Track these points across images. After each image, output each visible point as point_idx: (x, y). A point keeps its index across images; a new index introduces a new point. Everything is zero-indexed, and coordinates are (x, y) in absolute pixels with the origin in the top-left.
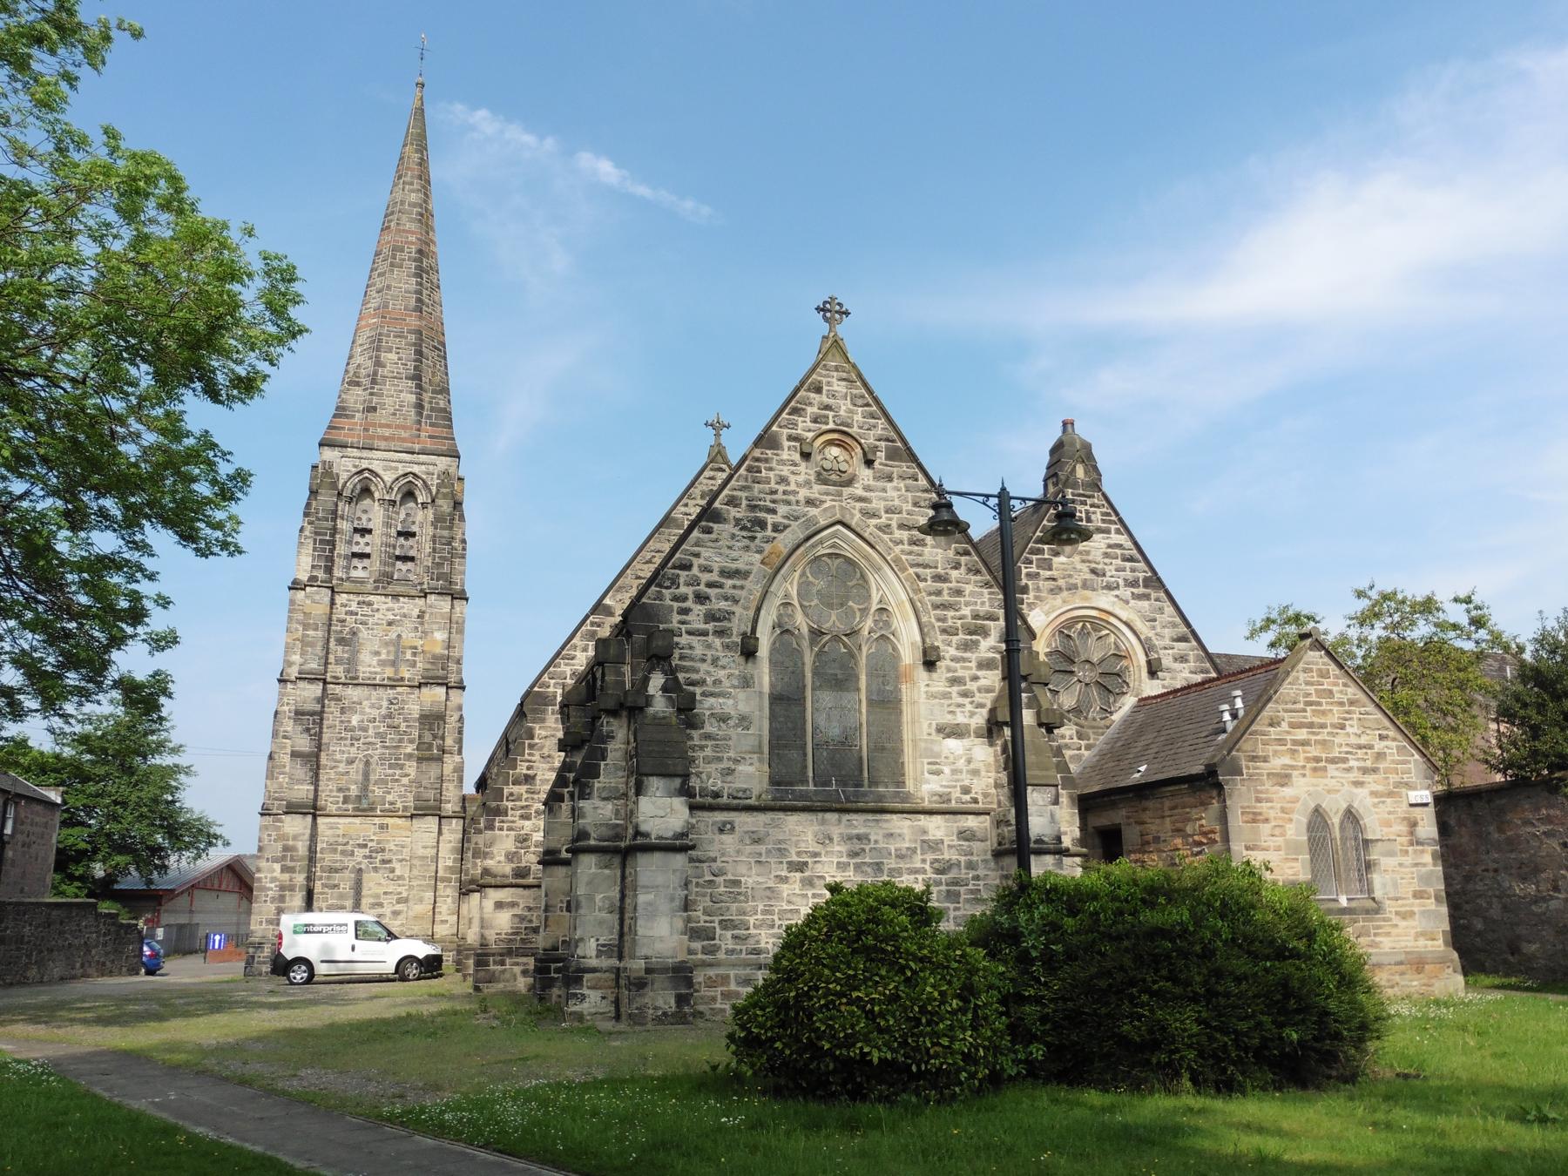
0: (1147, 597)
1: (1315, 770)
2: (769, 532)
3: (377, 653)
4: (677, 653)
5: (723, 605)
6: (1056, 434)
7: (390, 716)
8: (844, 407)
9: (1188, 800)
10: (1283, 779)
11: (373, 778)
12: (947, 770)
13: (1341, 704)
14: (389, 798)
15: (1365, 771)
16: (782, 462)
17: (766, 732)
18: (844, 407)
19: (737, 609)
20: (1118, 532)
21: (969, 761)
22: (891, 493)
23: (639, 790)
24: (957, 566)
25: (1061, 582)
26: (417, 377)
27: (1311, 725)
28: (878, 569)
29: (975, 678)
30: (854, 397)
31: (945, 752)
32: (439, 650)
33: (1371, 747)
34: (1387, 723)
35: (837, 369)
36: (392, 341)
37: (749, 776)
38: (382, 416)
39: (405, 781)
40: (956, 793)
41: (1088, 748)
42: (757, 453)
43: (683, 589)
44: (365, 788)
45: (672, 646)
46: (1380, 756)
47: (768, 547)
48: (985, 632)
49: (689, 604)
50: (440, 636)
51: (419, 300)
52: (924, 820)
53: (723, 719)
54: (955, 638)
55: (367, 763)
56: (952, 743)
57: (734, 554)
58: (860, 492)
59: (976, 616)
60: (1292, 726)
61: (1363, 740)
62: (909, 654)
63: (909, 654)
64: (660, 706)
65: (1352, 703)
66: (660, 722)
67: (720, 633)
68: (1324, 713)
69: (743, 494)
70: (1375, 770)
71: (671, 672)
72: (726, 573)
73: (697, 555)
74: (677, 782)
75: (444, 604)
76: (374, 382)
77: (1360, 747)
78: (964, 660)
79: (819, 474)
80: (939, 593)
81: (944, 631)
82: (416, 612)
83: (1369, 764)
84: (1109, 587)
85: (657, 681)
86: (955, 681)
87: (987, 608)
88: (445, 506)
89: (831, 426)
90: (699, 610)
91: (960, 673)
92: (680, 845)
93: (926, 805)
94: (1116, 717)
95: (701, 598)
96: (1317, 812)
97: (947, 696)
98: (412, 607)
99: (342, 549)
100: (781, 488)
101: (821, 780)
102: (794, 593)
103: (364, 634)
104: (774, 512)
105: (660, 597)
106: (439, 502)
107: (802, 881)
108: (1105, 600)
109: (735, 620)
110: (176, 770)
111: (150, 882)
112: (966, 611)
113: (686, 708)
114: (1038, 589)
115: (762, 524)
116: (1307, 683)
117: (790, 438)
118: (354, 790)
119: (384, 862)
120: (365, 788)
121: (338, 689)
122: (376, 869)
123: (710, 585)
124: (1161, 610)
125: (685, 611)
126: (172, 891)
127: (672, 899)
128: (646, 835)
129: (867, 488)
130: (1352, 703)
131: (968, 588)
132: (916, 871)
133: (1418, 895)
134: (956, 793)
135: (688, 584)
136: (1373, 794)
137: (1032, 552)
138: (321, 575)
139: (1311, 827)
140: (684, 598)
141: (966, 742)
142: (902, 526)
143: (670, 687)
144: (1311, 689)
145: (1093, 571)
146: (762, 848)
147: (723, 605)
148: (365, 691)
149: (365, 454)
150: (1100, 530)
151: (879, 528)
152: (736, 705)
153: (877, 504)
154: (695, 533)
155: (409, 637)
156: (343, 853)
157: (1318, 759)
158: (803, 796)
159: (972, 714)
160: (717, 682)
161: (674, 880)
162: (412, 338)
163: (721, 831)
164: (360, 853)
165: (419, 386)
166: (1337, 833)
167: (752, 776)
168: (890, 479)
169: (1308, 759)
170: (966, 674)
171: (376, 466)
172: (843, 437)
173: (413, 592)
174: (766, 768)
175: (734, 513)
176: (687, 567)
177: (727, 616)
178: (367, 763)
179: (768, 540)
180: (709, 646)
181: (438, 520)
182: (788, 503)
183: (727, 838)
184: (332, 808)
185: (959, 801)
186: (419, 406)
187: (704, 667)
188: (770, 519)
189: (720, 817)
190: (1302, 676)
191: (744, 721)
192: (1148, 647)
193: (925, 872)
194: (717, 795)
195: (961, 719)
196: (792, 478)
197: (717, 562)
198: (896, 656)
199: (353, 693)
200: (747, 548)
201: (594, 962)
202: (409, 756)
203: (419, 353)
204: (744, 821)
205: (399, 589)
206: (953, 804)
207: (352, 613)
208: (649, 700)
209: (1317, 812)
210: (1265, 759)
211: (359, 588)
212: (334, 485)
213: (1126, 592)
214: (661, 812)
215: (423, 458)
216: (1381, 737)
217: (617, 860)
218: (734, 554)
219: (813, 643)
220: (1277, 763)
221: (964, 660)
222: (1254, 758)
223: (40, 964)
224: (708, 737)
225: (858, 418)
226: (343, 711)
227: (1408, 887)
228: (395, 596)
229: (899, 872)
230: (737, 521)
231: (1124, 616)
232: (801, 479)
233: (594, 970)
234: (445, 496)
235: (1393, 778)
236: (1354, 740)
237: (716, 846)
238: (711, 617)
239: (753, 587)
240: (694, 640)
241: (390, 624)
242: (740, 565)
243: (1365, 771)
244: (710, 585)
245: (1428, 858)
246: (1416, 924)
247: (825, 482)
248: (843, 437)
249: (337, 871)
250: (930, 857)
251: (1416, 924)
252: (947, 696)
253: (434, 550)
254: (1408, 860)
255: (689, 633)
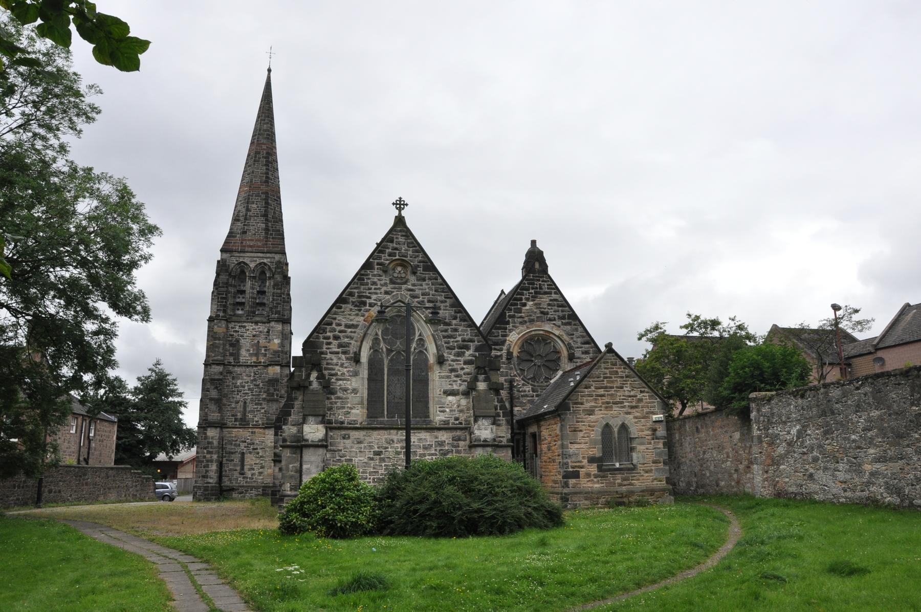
0: (569, 324)
1: (606, 408)
2: (367, 307)
3: (248, 350)
4: (325, 362)
5: (346, 340)
6: (528, 246)
7: (255, 380)
8: (404, 248)
9: (553, 422)
10: (591, 412)
11: (248, 409)
12: (448, 410)
13: (622, 377)
14: (256, 419)
15: (632, 407)
16: (375, 275)
17: (366, 395)
18: (404, 248)
19: (353, 342)
20: (555, 293)
21: (458, 406)
22: (425, 286)
23: (304, 422)
24: (455, 318)
25: (526, 319)
26: (265, 215)
27: (606, 387)
28: (419, 321)
29: (462, 369)
30: (408, 244)
31: (447, 402)
32: (276, 348)
33: (636, 396)
34: (644, 385)
35: (401, 231)
36: (254, 199)
37: (357, 415)
38: (249, 235)
39: (263, 411)
40: (452, 421)
41: (537, 396)
42: (363, 272)
43: (328, 334)
44: (244, 414)
45: (321, 359)
46: (640, 400)
47: (367, 314)
48: (468, 348)
49: (331, 340)
50: (277, 341)
51: (267, 177)
52: (436, 433)
53: (346, 390)
54: (453, 351)
55: (245, 403)
56: (450, 398)
57: (352, 318)
58: (410, 287)
59: (464, 341)
60: (597, 388)
61: (632, 393)
62: (432, 359)
63: (432, 359)
64: (315, 385)
65: (627, 377)
66: (314, 393)
67: (344, 353)
68: (612, 382)
69: (356, 291)
70: (636, 407)
71: (320, 370)
72: (347, 326)
73: (335, 319)
74: (320, 418)
75: (279, 327)
76: (246, 219)
77: (630, 396)
78: (458, 361)
79: (391, 280)
80: (446, 331)
81: (448, 348)
82: (266, 330)
83: (634, 404)
84: (550, 320)
85: (314, 375)
86: (452, 370)
87: (469, 336)
88: (278, 278)
89: (397, 257)
90: (335, 342)
91: (455, 367)
92: (323, 444)
93: (437, 425)
94: (552, 381)
95: (336, 338)
96: (607, 425)
97: (448, 377)
98: (262, 328)
99: (230, 301)
100: (373, 287)
101: (391, 415)
102: (380, 333)
103: (242, 341)
104: (370, 298)
105: (318, 338)
106: (276, 276)
107: (380, 459)
108: (547, 327)
109: (352, 346)
110: (180, 404)
111: (171, 457)
112: (459, 339)
113: (327, 388)
114: (514, 323)
115: (364, 304)
116: (606, 368)
117: (378, 264)
118: (239, 416)
119: (254, 449)
120: (244, 414)
121: (231, 368)
122: (250, 453)
123: (340, 332)
124: (577, 330)
125: (329, 344)
126: (182, 462)
127: (318, 467)
128: (307, 440)
129: (414, 285)
130: (627, 377)
131: (460, 328)
132: (432, 455)
133: (654, 462)
134: (452, 421)
135: (330, 332)
136: (636, 418)
137: (512, 305)
138: (221, 314)
139: (603, 433)
140: (328, 338)
141: (458, 397)
142: (429, 301)
143: (321, 377)
144: (607, 371)
145: (542, 313)
146: (362, 445)
147: (346, 340)
148: (244, 369)
149: (242, 255)
150: (546, 293)
151: (419, 303)
152: (351, 385)
153: (418, 292)
154: (334, 309)
155: (262, 342)
156: (235, 445)
157: (608, 403)
158: (381, 423)
159: (460, 385)
160: (343, 374)
161: (320, 459)
162: (263, 196)
163: (344, 438)
164: (243, 445)
165: (267, 220)
166: (616, 435)
167: (358, 414)
168: (424, 280)
169: (603, 403)
170: (459, 367)
171: (247, 260)
172: (403, 264)
173: (265, 320)
174: (365, 411)
175: (351, 299)
176: (331, 324)
177: (347, 345)
178: (245, 403)
179: (367, 311)
180: (340, 359)
181: (276, 285)
182: (376, 293)
183: (347, 441)
184: (230, 424)
185: (453, 424)
186: (267, 230)
187: (337, 368)
188: (368, 301)
189: (343, 432)
190: (603, 365)
191: (355, 391)
192: (569, 347)
193: (436, 455)
194: (342, 423)
195: (455, 387)
196: (379, 282)
197: (344, 321)
198: (427, 359)
199: (238, 370)
200: (357, 315)
201: (289, 493)
202: (264, 399)
203: (267, 203)
204: (355, 434)
205: (258, 319)
206: (451, 425)
207: (236, 331)
208: (310, 383)
209: (607, 425)
210: (582, 404)
211: (239, 319)
212: (227, 271)
213: (559, 323)
214: (314, 431)
215: (268, 255)
216: (641, 392)
217: (299, 451)
218: (352, 318)
219: (388, 355)
220: (587, 405)
221: (458, 361)
222: (576, 403)
223: (105, 494)
224: (339, 398)
225: (410, 253)
226: (233, 378)
227: (651, 457)
228: (256, 323)
229: (424, 455)
230: (353, 302)
231: (557, 333)
232: (383, 282)
233: (289, 496)
234: (279, 273)
235: (646, 410)
236: (627, 393)
237: (342, 445)
238: (340, 346)
239: (360, 332)
240: (333, 356)
241: (254, 336)
242: (355, 323)
243: (632, 407)
244: (340, 332)
245: (661, 445)
246: (653, 475)
247: (394, 283)
248: (403, 264)
249: (232, 453)
250: (438, 449)
251: (653, 475)
252: (448, 377)
253: (273, 300)
254: (650, 446)
255: (331, 353)
